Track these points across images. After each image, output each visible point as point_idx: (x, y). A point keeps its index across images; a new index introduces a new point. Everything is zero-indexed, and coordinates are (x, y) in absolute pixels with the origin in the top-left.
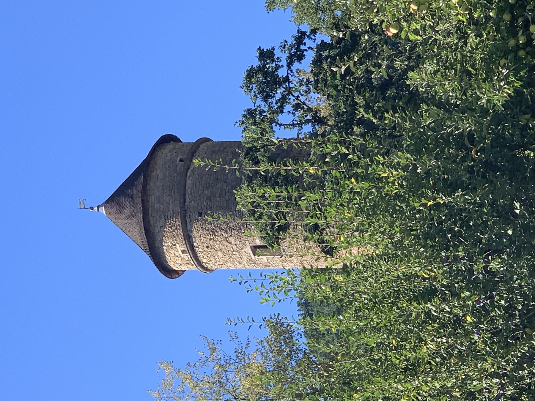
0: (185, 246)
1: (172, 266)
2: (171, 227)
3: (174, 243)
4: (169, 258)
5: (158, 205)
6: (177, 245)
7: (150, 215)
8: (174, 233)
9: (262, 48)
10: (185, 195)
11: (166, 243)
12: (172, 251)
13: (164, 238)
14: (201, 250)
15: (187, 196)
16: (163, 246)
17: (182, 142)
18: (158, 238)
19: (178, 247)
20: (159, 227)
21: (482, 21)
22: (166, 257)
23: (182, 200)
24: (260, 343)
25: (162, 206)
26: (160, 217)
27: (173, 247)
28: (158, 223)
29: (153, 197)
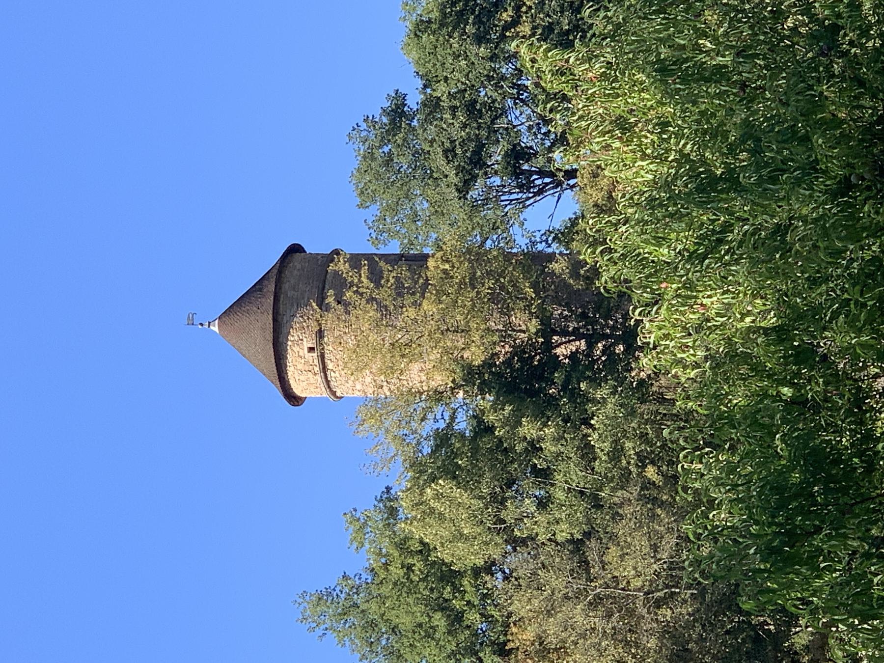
0: (314, 341)
1: (290, 374)
2: (302, 317)
3: (301, 338)
4: (290, 361)
5: (293, 292)
6: (305, 340)
7: (281, 302)
8: (304, 324)
9: (358, 201)
10: (325, 281)
11: (293, 336)
12: (296, 349)
13: (291, 330)
14: (331, 349)
15: (327, 283)
16: (287, 340)
17: (305, 252)
18: (284, 331)
19: (305, 343)
20: (288, 316)
21: (875, 304)
22: (287, 358)
23: (321, 286)
24: (421, 188)
25: (296, 294)
26: (292, 305)
27: (300, 342)
28: (288, 311)
29: (288, 283)
